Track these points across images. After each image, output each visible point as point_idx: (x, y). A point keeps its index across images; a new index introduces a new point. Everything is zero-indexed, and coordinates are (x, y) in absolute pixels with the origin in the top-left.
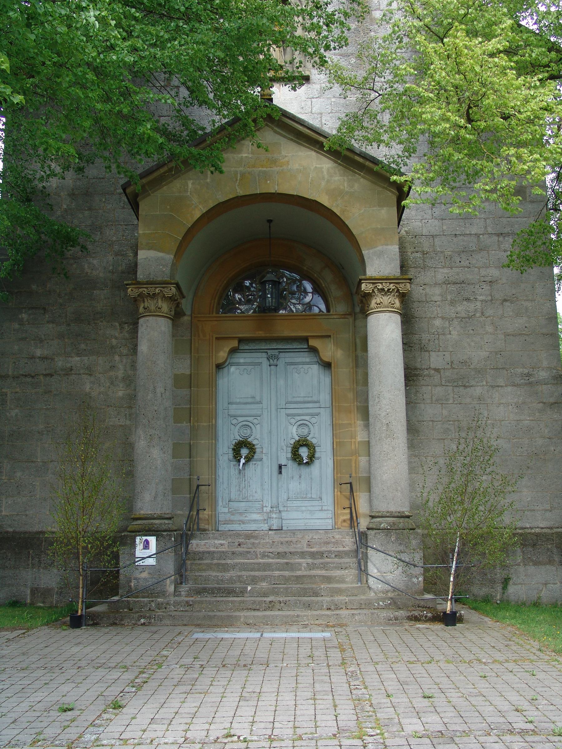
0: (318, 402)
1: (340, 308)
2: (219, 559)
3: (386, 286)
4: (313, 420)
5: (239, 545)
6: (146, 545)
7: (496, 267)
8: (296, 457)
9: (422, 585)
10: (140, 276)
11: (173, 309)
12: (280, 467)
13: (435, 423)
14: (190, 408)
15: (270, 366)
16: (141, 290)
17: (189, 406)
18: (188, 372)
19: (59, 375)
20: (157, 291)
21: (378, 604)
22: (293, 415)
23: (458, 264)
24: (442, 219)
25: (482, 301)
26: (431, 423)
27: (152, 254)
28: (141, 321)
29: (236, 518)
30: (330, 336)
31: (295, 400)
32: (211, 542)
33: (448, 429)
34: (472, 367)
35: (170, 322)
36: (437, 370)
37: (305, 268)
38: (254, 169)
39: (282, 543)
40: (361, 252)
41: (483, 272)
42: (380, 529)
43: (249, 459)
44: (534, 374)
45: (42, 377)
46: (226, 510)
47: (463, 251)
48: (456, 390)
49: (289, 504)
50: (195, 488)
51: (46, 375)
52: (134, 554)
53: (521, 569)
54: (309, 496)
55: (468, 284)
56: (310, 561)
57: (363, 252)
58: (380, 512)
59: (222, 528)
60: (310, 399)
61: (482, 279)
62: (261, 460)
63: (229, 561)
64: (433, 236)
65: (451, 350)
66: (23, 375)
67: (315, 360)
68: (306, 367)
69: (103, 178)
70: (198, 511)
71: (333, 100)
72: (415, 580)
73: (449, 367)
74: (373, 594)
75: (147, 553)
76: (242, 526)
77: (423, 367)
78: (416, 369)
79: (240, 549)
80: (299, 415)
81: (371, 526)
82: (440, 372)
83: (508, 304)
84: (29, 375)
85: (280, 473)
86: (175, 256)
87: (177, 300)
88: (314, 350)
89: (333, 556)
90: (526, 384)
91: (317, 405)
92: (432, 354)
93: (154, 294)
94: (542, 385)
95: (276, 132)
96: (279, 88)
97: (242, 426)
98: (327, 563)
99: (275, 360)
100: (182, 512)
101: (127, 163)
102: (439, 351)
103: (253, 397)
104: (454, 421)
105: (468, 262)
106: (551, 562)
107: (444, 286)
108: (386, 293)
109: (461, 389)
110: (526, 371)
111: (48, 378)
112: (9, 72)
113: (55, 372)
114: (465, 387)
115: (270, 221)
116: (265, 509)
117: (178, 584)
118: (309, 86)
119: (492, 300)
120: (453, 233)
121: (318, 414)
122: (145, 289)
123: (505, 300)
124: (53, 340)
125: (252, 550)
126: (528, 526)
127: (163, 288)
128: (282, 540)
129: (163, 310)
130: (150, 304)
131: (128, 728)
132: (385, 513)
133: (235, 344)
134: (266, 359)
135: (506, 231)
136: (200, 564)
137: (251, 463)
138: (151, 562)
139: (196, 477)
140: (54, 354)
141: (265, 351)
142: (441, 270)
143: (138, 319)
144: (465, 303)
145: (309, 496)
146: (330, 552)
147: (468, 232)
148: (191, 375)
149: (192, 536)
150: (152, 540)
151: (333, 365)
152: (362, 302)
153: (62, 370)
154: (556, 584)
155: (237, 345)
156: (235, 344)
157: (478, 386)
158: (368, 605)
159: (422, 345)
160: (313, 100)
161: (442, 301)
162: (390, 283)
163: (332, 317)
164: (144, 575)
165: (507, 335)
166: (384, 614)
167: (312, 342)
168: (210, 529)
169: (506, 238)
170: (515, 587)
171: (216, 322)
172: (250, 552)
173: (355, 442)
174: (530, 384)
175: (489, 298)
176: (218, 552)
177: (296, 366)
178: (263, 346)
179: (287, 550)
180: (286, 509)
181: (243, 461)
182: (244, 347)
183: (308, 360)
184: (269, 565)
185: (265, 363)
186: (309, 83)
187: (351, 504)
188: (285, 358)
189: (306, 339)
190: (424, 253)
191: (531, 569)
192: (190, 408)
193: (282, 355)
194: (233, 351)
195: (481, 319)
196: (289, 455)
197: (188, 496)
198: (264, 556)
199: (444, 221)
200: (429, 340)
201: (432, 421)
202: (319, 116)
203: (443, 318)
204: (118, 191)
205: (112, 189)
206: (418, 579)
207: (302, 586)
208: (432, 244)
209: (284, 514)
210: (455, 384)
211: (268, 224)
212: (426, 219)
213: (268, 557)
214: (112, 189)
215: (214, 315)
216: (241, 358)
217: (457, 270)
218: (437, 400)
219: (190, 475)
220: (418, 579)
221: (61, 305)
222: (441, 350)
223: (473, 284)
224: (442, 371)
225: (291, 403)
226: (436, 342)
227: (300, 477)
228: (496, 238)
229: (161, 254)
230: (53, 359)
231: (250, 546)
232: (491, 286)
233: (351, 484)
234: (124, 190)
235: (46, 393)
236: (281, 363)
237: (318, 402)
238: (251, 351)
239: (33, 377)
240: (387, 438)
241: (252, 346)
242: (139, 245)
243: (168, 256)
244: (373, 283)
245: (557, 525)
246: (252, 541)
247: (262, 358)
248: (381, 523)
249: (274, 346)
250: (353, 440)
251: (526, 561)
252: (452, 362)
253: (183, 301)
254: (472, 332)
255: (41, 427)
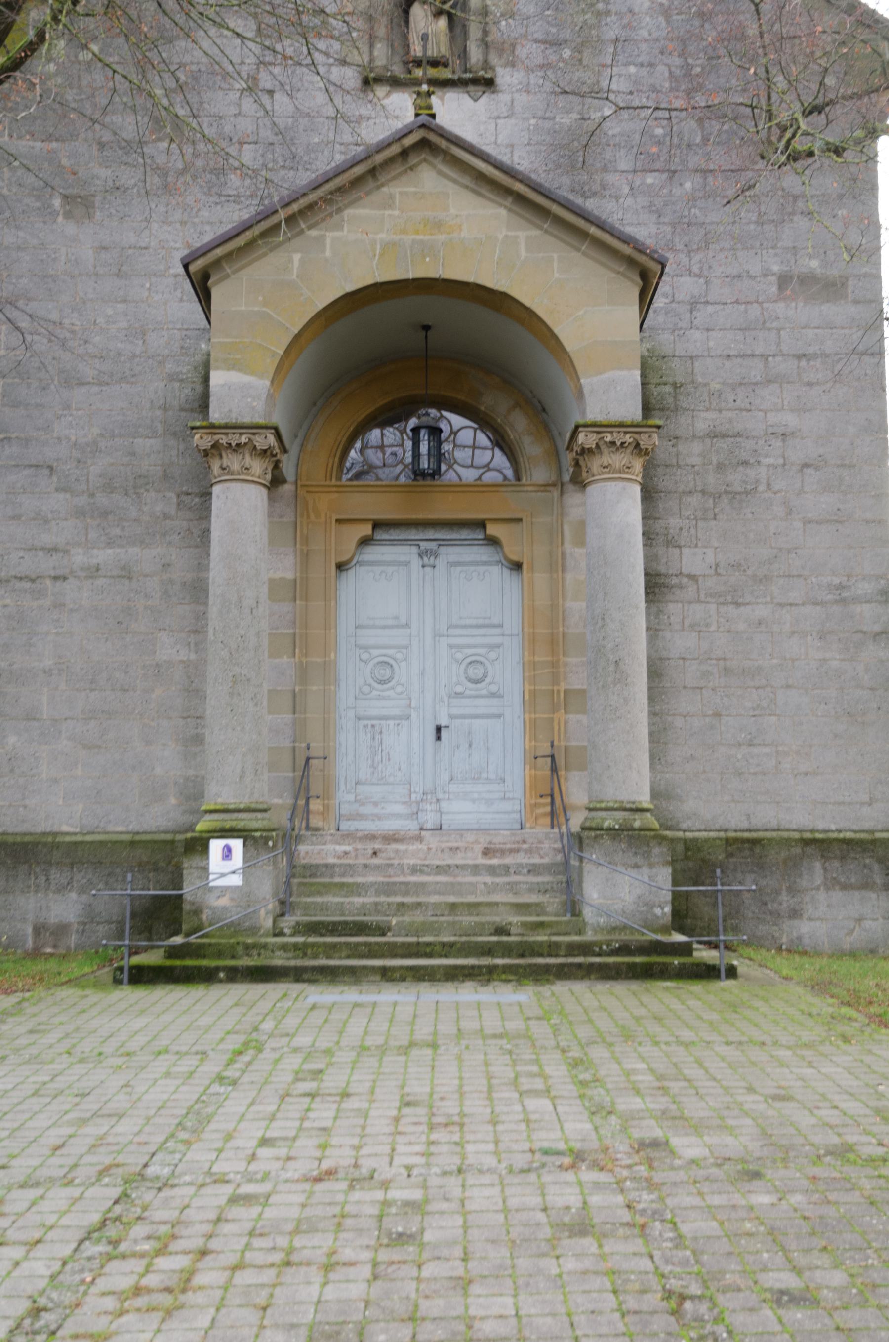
0: (501, 626)
1: (539, 474)
2: (343, 875)
3: (619, 438)
4: (493, 655)
5: (375, 853)
6: (227, 853)
7: (792, 411)
9: (669, 918)
10: (216, 415)
11: (269, 470)
12: (438, 729)
13: (687, 663)
14: (295, 634)
15: (423, 566)
16: (216, 437)
17: (292, 631)
18: (290, 575)
19: (78, 577)
20: (244, 439)
21: (601, 948)
22: (460, 647)
23: (731, 405)
24: (708, 330)
25: (769, 466)
26: (681, 662)
27: (234, 377)
28: (216, 490)
29: (368, 810)
30: (520, 520)
31: (463, 622)
32: (330, 847)
33: (707, 671)
34: (749, 572)
35: (264, 491)
36: (693, 577)
37: (482, 408)
38: (403, 236)
39: (442, 851)
40: (579, 380)
41: (772, 418)
42: (602, 829)
44: (850, 586)
45: (48, 582)
46: (351, 797)
47: (741, 384)
48: (723, 609)
49: (453, 788)
50: (303, 763)
51: (56, 578)
52: (206, 869)
53: (822, 895)
54: (484, 775)
55: (747, 438)
56: (489, 880)
57: (582, 381)
58: (602, 802)
59: (345, 826)
60: (487, 621)
61: (770, 430)
63: (360, 880)
64: (691, 358)
65: (716, 544)
66: (16, 577)
67: (497, 558)
68: (482, 569)
69: (146, 248)
70: (308, 799)
71: (533, 122)
72: (658, 911)
73: (712, 572)
76: (377, 822)
77: (670, 572)
78: (659, 575)
79: (376, 861)
80: (469, 646)
81: (588, 824)
82: (697, 581)
83: (809, 471)
84: (26, 577)
85: (439, 738)
86: (272, 382)
87: (275, 455)
89: (525, 871)
90: (836, 602)
91: (497, 631)
92: (686, 551)
93: (238, 445)
94: (861, 603)
95: (440, 173)
96: (442, 99)
97: (378, 663)
98: (517, 883)
99: (432, 558)
100: (281, 800)
101: (186, 223)
102: (696, 546)
104: (718, 659)
105: (747, 401)
106: (866, 885)
107: (708, 441)
108: (618, 449)
109: (731, 608)
110: (836, 581)
111: (58, 583)
113: (72, 572)
114: (737, 604)
115: (426, 328)
116: (413, 796)
118: (493, 96)
119: (784, 465)
120: (726, 352)
121: (498, 646)
122: (223, 437)
123: (806, 465)
124: (66, 520)
125: (396, 862)
126: (833, 827)
127: (254, 434)
128: (444, 845)
129: (253, 471)
130: (233, 461)
131: (223, 1156)
132: (611, 804)
133: (367, 530)
134: (416, 556)
135: (811, 350)
136: (312, 884)
138: (236, 880)
139: (304, 745)
140: (67, 544)
141: (415, 543)
142: (703, 414)
143: (212, 485)
144: (741, 468)
145: (484, 775)
146: (520, 865)
147: (749, 352)
148: (295, 580)
149: (299, 839)
150: (237, 845)
151: (525, 567)
152: (577, 464)
153: (82, 569)
154: (877, 919)
155: (370, 532)
156: (367, 530)
157: (758, 603)
159: (670, 537)
160: (499, 121)
161: (704, 464)
162: (626, 433)
163: (525, 489)
164: (224, 902)
165: (807, 522)
167: (492, 530)
168: (326, 828)
169: (812, 363)
170: (812, 924)
171: (336, 495)
172: (392, 865)
173: (558, 691)
174: (843, 601)
175: (781, 461)
176: (341, 865)
177: (465, 568)
178: (413, 534)
179: (450, 861)
180: (447, 796)
182: (380, 535)
183: (484, 558)
184: (423, 885)
185: (416, 562)
186: (493, 92)
187: (552, 789)
188: (449, 554)
189: (482, 525)
190: (675, 386)
191: (838, 895)
192: (295, 634)
193: (443, 550)
194: (365, 541)
195: (766, 495)
197: (291, 775)
198: (414, 870)
199: (710, 333)
200: (681, 529)
201: (684, 659)
202: (509, 150)
203: (703, 492)
204: (172, 271)
205: (162, 267)
206: (662, 909)
207: (477, 919)
208: (690, 371)
209: (444, 805)
210: (722, 600)
211: (424, 333)
212: (681, 329)
213: (422, 872)
214: (162, 267)
215: (334, 482)
216: (372, 553)
217: (730, 414)
218: (692, 626)
219: (294, 741)
220: (662, 909)
221: (79, 461)
222: (700, 544)
223: (754, 437)
224: (700, 580)
225: (457, 626)
226: (693, 531)
227: (470, 745)
228: (796, 362)
229: (247, 379)
230: (66, 552)
231: (392, 855)
232: (784, 441)
233: (552, 757)
234: (186, 267)
235: (55, 607)
236: (441, 562)
237: (501, 626)
238: (393, 542)
239: (33, 581)
240: (615, 685)
241: (394, 534)
242: (212, 362)
243: (262, 382)
244: (598, 433)
245: (879, 827)
246: (394, 846)
247: (408, 553)
248: (604, 819)
249: (431, 534)
250: (555, 688)
251: (831, 884)
252: (717, 565)
253: (284, 458)
254: (750, 516)
255: (48, 663)
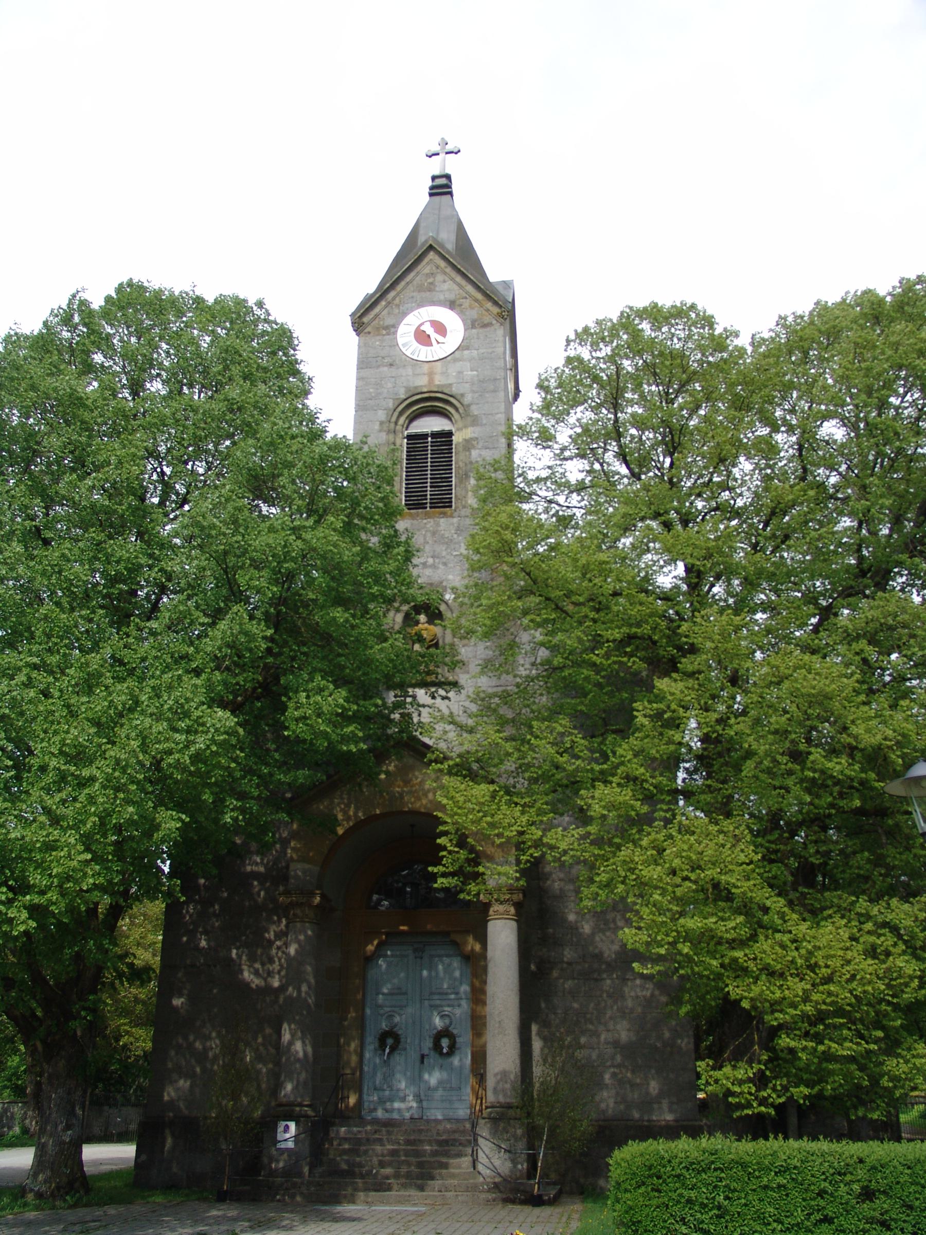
6: (287, 1129)
8: (437, 1047)
12: (423, 1057)
43: (393, 1049)
62: (405, 1049)
74: (481, 1179)
75: (287, 1136)
88: (455, 944)
103: (399, 989)
112: (167, 1132)
115: (412, 826)
117: (312, 1167)
137: (396, 1053)
138: (291, 1145)
158: (474, 1188)
166: (483, 1196)
181: (387, 1050)
189: (447, 934)
196: (431, 1045)
